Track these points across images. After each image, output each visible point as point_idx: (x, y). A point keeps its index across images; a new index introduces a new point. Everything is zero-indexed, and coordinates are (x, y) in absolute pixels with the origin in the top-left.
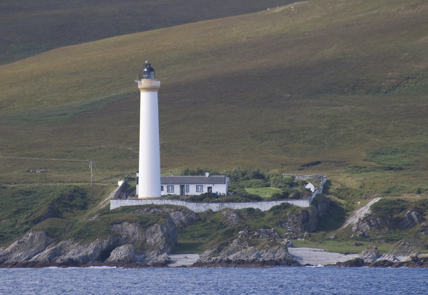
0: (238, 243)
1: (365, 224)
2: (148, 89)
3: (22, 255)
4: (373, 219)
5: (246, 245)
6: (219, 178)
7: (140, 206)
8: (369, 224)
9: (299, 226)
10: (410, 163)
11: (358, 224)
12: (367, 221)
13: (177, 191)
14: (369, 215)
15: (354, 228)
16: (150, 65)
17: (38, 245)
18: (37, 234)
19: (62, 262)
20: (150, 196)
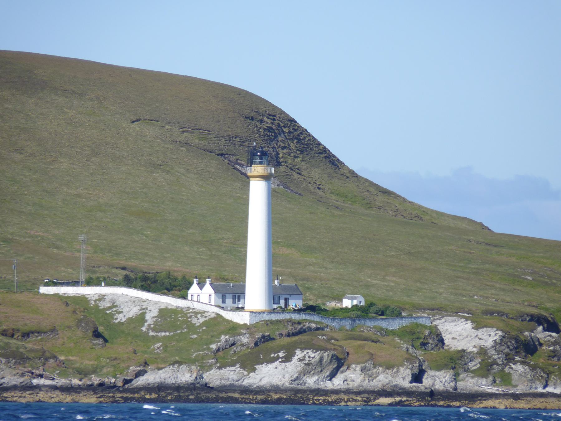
1: (504, 347)
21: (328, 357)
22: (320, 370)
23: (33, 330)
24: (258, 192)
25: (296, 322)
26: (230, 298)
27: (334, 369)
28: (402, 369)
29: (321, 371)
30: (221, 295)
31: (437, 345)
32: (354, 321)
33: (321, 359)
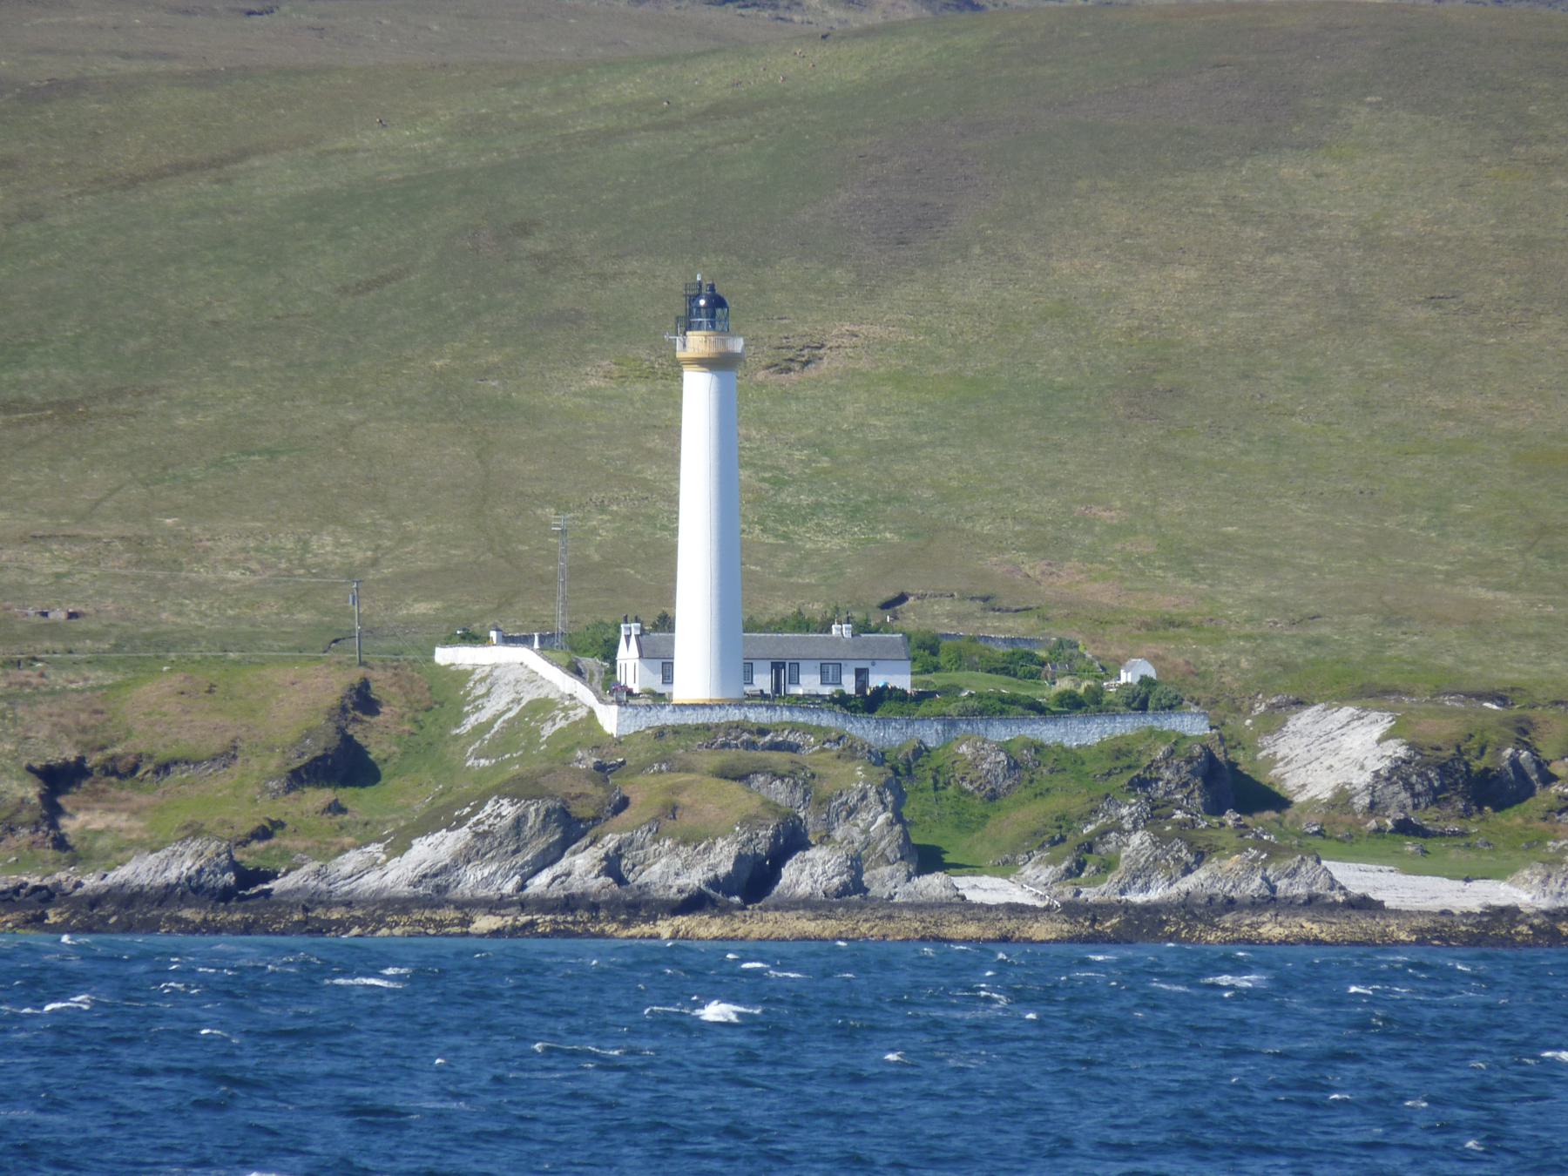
0: (1154, 843)
1: (1396, 788)
2: (706, 363)
3: (495, 873)
4: (1420, 775)
5: (1180, 850)
6: (886, 640)
7: (707, 727)
8: (1409, 786)
9: (1196, 794)
10: (1190, 618)
11: (1371, 788)
12: (1402, 779)
13: (763, 682)
14: (1404, 761)
15: (1363, 801)
16: (712, 288)
17: (540, 844)
18: (537, 810)
19: (685, 895)
20: (716, 696)
21: (537, 815)
22: (512, 848)
23: (178, 756)
24: (698, 393)
25: (754, 729)
26: (810, 673)
27: (554, 844)
28: (720, 843)
29: (515, 852)
30: (659, 663)
31: (1186, 785)
32: (951, 724)
33: (519, 822)
